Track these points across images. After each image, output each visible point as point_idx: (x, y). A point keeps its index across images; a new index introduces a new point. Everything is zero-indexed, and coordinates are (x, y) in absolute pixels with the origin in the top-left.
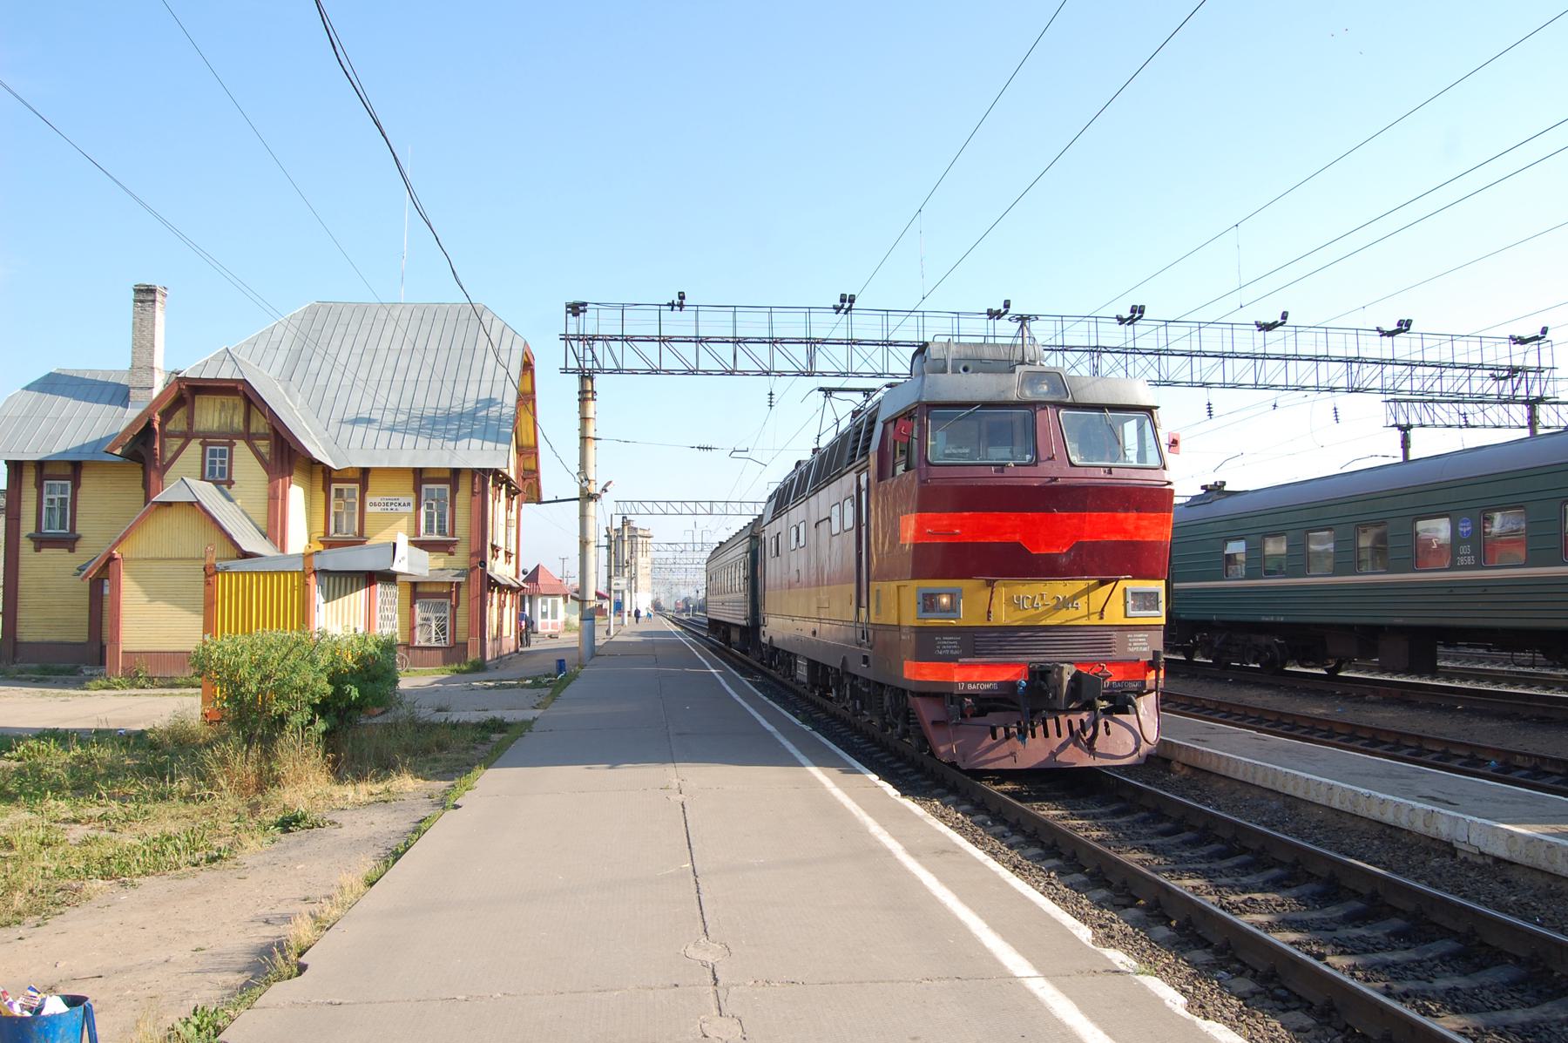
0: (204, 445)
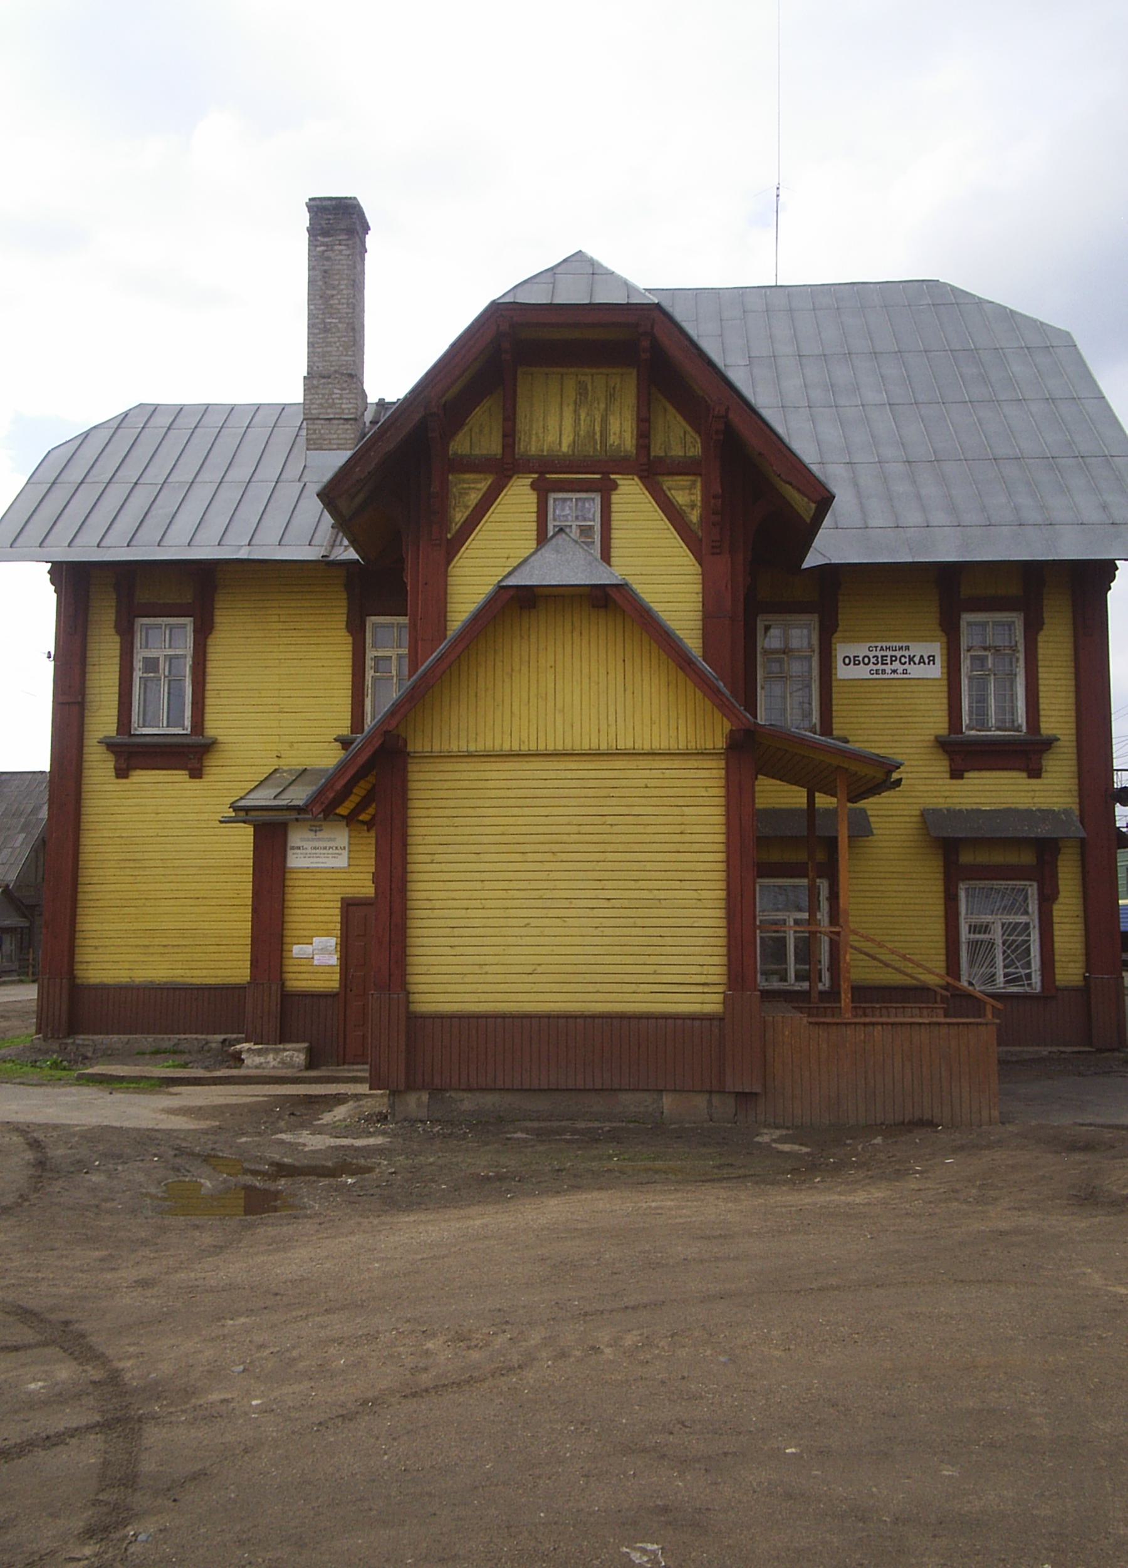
0: (543, 490)
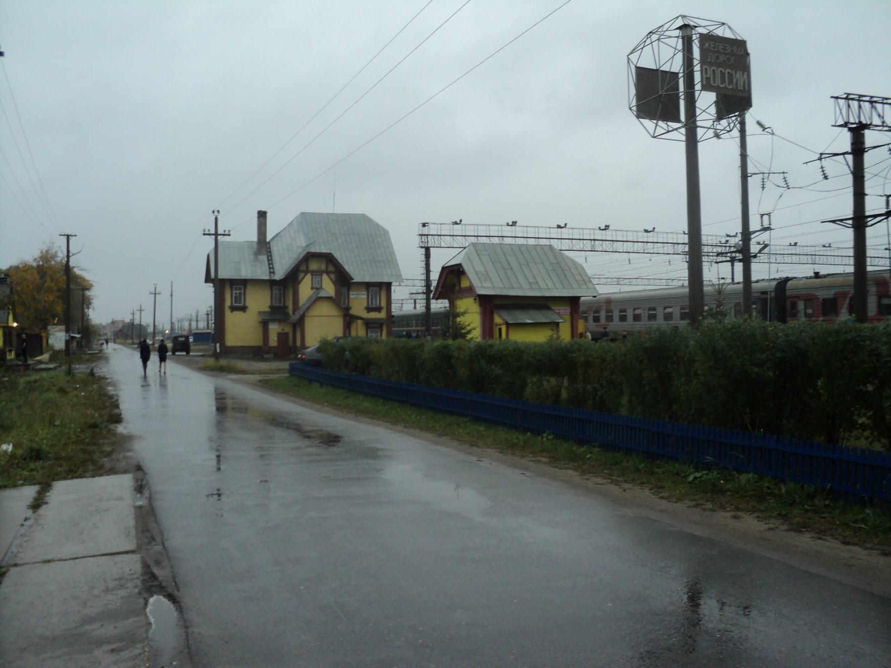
0: (312, 275)
